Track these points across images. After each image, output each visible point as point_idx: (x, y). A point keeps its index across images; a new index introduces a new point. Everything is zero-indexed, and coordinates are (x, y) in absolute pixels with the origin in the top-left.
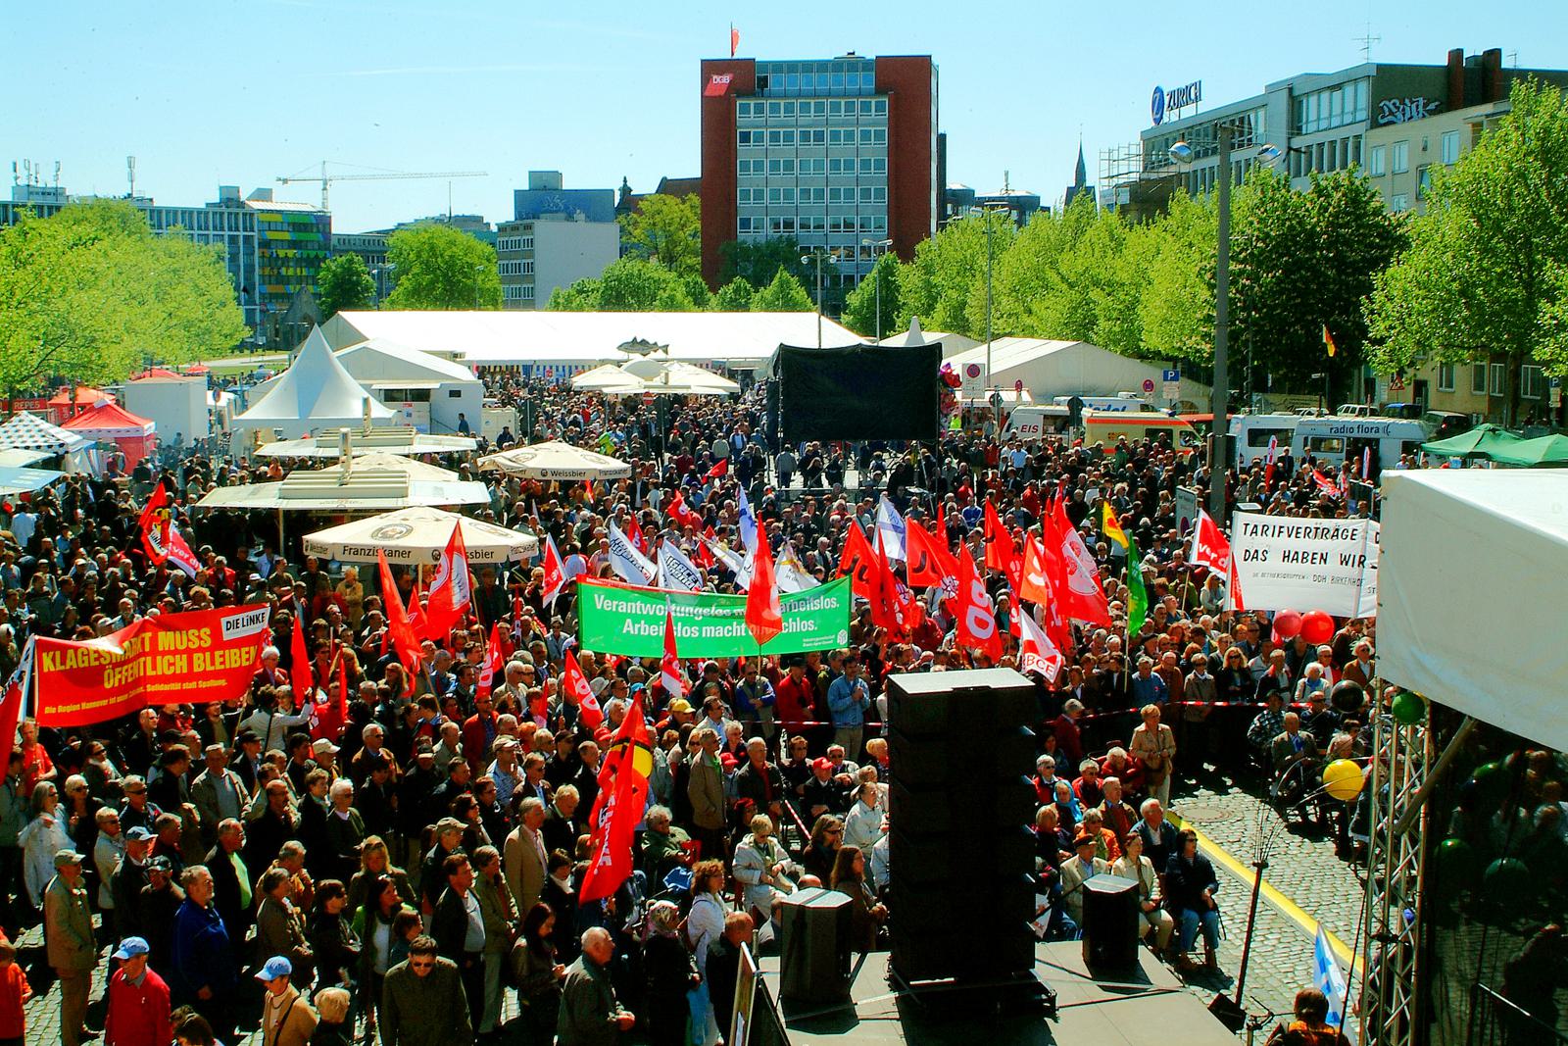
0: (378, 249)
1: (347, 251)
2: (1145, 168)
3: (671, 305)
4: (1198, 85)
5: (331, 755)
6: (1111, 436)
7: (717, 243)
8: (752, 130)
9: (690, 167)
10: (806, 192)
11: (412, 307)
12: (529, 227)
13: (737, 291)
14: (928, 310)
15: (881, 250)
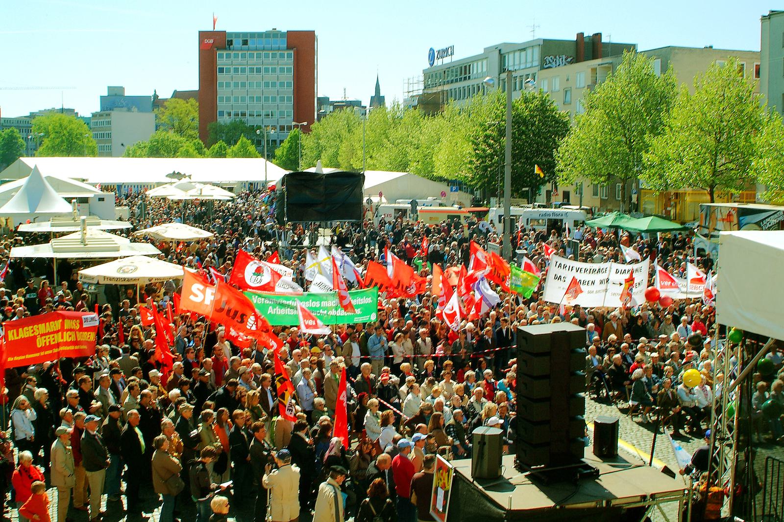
0: (25, 125)
1: (11, 126)
2: (425, 88)
3: (187, 155)
4: (452, 48)
5: (158, 377)
6: (431, 218)
7: (209, 124)
8: (240, 67)
9: (192, 83)
10: (252, 98)
11: (48, 155)
12: (109, 115)
13: (220, 147)
14: (319, 157)
15: (289, 128)
